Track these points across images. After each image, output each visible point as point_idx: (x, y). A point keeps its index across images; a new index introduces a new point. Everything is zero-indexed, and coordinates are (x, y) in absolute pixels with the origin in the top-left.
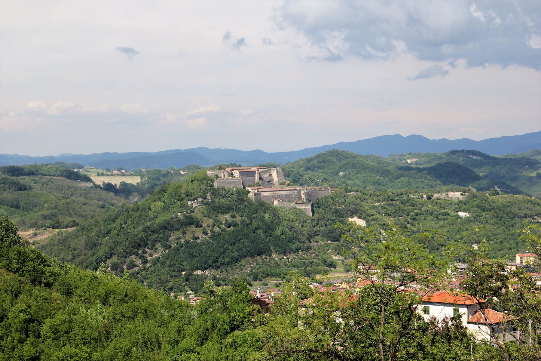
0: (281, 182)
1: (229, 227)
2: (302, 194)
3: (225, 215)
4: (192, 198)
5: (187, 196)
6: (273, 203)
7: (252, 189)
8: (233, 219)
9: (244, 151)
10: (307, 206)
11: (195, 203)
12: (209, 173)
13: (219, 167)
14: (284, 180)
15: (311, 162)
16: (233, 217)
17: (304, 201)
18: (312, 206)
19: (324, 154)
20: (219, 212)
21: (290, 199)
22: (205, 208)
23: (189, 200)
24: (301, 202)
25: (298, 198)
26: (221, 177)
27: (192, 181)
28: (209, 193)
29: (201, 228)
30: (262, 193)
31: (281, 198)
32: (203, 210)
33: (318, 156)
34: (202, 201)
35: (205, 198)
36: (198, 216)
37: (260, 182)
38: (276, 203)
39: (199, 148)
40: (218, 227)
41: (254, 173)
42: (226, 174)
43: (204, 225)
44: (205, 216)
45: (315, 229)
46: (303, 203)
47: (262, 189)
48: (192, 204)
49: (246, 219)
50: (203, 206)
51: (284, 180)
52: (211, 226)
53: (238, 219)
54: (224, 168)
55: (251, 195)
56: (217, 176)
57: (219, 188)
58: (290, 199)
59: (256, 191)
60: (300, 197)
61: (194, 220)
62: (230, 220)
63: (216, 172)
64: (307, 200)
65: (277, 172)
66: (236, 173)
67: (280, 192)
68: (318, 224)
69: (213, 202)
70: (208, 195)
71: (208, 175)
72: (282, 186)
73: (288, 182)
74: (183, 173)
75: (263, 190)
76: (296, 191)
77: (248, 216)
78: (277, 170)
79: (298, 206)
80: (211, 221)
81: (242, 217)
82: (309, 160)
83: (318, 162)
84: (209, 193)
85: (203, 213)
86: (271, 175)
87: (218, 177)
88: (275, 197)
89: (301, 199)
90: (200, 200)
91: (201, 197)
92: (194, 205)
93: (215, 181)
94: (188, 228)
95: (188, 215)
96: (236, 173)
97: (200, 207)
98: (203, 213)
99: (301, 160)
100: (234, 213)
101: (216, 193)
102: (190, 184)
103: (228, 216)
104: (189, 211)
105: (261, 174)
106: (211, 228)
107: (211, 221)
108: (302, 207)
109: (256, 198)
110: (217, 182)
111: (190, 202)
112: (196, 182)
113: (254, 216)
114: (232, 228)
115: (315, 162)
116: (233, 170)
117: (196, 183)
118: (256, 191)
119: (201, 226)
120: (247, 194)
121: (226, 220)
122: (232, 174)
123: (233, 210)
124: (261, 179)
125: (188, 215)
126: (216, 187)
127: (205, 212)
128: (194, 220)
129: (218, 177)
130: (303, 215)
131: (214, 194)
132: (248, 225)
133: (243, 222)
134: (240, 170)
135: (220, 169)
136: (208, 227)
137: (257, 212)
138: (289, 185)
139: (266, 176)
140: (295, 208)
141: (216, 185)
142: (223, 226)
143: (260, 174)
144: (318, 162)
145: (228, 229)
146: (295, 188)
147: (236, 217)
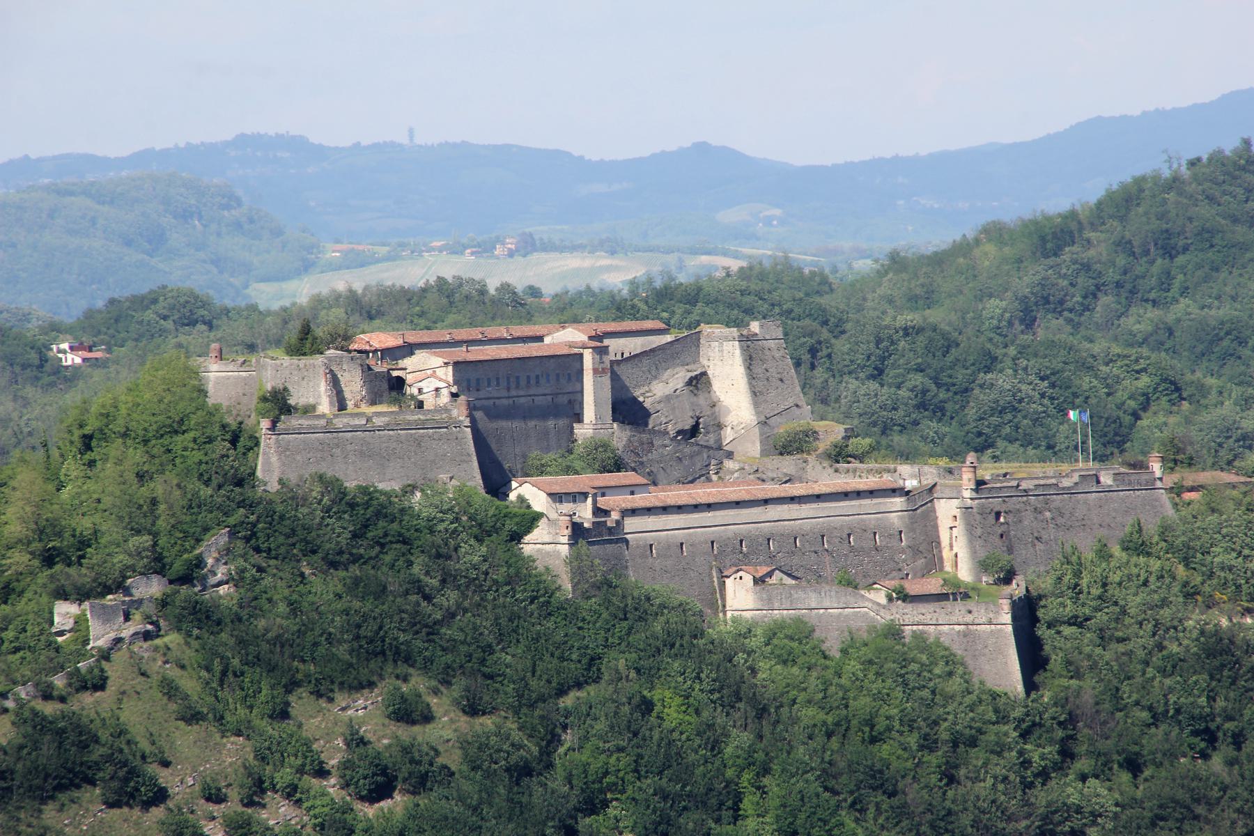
0: (783, 428)
1: (380, 792)
2: (944, 522)
3: (341, 699)
4: (81, 575)
5: (49, 559)
6: (716, 599)
7: (557, 497)
8: (405, 733)
9: (593, 154)
10: (980, 614)
11: (105, 615)
12: (224, 380)
13: (292, 335)
14: (804, 418)
15: (1068, 253)
16: (408, 712)
17: (965, 574)
18: (1026, 614)
19: (1175, 183)
20: (292, 686)
21: (848, 561)
22: (189, 655)
23: (62, 594)
24: (933, 585)
25: (915, 551)
26: (309, 410)
27: (87, 442)
28: (220, 538)
29: (157, 813)
30: (631, 524)
31: (774, 558)
32: (172, 672)
33: (1124, 201)
34: (163, 603)
35: (191, 574)
36: (133, 716)
37: (619, 436)
38: (740, 597)
39: (243, 141)
40: (291, 792)
41: (569, 364)
42: (353, 385)
43: (180, 783)
44: (192, 717)
45: (1041, 797)
46: (955, 593)
47: (632, 489)
48: (80, 621)
49: (512, 725)
50: (172, 639)
51: (804, 418)
52: (234, 795)
53: (447, 729)
54: (342, 339)
55: (547, 545)
56: (279, 404)
57: (291, 495)
58: (848, 561)
59: (585, 513)
60: (927, 548)
61: (97, 753)
62: (384, 736)
63: (275, 369)
64: (983, 566)
65: (750, 360)
66: (430, 376)
67: (774, 512)
68: (1067, 754)
69: (253, 604)
70: (211, 548)
71: (216, 396)
72: (788, 465)
73: (832, 432)
74: (72, 359)
75: (640, 500)
76: (898, 502)
77: (524, 702)
78: (747, 341)
79: (912, 618)
80: (233, 754)
81: (473, 710)
82: (1052, 237)
83: (1124, 245)
84: (220, 538)
85: (170, 690)
86: (699, 382)
87: (287, 409)
88: (735, 554)
89: (934, 563)
90: (150, 588)
91: (158, 566)
92: (100, 637)
93: (268, 442)
94: (49, 811)
95: (49, 709)
96: (430, 376)
97: (142, 647)
98: (170, 690)
99: (995, 232)
100: (419, 683)
101: (271, 531)
102: (72, 468)
103: (363, 711)
104: (59, 681)
105: (625, 372)
106: (233, 806)
107: (233, 754)
108: (941, 625)
109: (577, 566)
110: (283, 450)
111: (64, 613)
112: (115, 448)
113: (568, 701)
114: (398, 803)
115: (1099, 247)
116: (408, 349)
117: (121, 461)
118: (585, 513)
119: (161, 796)
120: (516, 537)
121: (356, 741)
122: (398, 385)
123: (408, 660)
124: (627, 410)
125: (49, 709)
126: (274, 486)
127: (190, 684)
128: (97, 753)
129: (287, 409)
130: (954, 685)
131: (248, 536)
132: (522, 772)
133: (477, 754)
134: (461, 354)
135: (305, 340)
136: (215, 797)
137: (591, 671)
138: (839, 455)
139: (659, 391)
140: (893, 632)
141: (272, 467)
142: (332, 786)
143: (614, 372)
144: (1124, 245)
145: (369, 811)
146: (887, 480)
147: (428, 718)
